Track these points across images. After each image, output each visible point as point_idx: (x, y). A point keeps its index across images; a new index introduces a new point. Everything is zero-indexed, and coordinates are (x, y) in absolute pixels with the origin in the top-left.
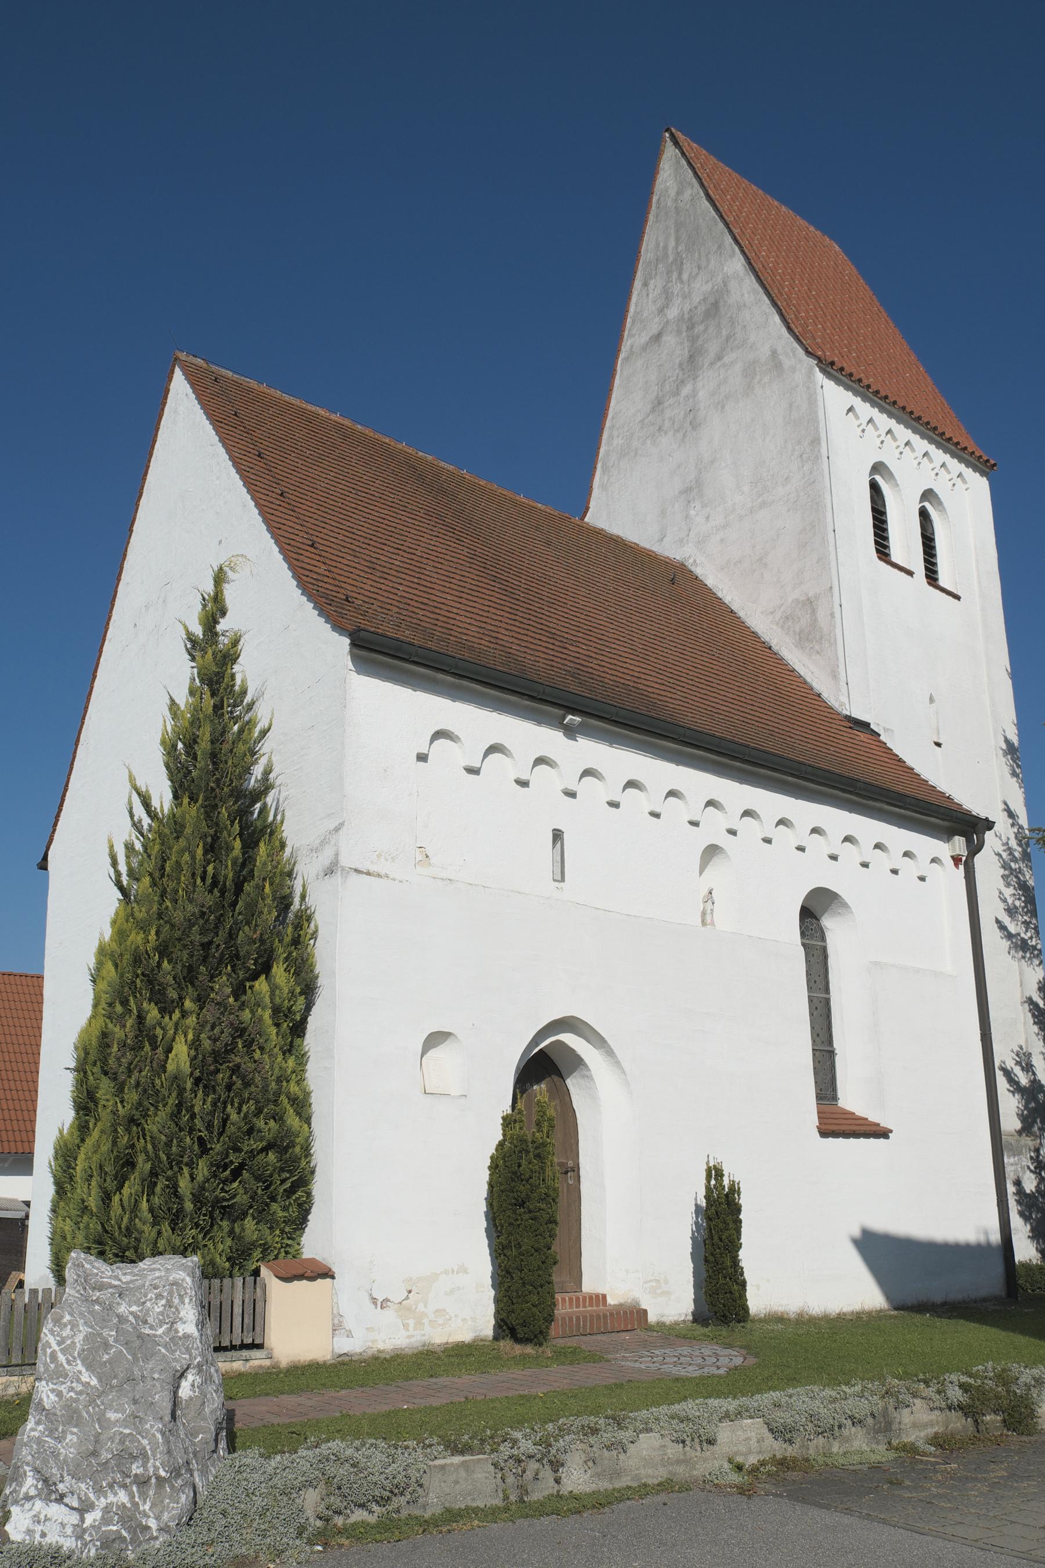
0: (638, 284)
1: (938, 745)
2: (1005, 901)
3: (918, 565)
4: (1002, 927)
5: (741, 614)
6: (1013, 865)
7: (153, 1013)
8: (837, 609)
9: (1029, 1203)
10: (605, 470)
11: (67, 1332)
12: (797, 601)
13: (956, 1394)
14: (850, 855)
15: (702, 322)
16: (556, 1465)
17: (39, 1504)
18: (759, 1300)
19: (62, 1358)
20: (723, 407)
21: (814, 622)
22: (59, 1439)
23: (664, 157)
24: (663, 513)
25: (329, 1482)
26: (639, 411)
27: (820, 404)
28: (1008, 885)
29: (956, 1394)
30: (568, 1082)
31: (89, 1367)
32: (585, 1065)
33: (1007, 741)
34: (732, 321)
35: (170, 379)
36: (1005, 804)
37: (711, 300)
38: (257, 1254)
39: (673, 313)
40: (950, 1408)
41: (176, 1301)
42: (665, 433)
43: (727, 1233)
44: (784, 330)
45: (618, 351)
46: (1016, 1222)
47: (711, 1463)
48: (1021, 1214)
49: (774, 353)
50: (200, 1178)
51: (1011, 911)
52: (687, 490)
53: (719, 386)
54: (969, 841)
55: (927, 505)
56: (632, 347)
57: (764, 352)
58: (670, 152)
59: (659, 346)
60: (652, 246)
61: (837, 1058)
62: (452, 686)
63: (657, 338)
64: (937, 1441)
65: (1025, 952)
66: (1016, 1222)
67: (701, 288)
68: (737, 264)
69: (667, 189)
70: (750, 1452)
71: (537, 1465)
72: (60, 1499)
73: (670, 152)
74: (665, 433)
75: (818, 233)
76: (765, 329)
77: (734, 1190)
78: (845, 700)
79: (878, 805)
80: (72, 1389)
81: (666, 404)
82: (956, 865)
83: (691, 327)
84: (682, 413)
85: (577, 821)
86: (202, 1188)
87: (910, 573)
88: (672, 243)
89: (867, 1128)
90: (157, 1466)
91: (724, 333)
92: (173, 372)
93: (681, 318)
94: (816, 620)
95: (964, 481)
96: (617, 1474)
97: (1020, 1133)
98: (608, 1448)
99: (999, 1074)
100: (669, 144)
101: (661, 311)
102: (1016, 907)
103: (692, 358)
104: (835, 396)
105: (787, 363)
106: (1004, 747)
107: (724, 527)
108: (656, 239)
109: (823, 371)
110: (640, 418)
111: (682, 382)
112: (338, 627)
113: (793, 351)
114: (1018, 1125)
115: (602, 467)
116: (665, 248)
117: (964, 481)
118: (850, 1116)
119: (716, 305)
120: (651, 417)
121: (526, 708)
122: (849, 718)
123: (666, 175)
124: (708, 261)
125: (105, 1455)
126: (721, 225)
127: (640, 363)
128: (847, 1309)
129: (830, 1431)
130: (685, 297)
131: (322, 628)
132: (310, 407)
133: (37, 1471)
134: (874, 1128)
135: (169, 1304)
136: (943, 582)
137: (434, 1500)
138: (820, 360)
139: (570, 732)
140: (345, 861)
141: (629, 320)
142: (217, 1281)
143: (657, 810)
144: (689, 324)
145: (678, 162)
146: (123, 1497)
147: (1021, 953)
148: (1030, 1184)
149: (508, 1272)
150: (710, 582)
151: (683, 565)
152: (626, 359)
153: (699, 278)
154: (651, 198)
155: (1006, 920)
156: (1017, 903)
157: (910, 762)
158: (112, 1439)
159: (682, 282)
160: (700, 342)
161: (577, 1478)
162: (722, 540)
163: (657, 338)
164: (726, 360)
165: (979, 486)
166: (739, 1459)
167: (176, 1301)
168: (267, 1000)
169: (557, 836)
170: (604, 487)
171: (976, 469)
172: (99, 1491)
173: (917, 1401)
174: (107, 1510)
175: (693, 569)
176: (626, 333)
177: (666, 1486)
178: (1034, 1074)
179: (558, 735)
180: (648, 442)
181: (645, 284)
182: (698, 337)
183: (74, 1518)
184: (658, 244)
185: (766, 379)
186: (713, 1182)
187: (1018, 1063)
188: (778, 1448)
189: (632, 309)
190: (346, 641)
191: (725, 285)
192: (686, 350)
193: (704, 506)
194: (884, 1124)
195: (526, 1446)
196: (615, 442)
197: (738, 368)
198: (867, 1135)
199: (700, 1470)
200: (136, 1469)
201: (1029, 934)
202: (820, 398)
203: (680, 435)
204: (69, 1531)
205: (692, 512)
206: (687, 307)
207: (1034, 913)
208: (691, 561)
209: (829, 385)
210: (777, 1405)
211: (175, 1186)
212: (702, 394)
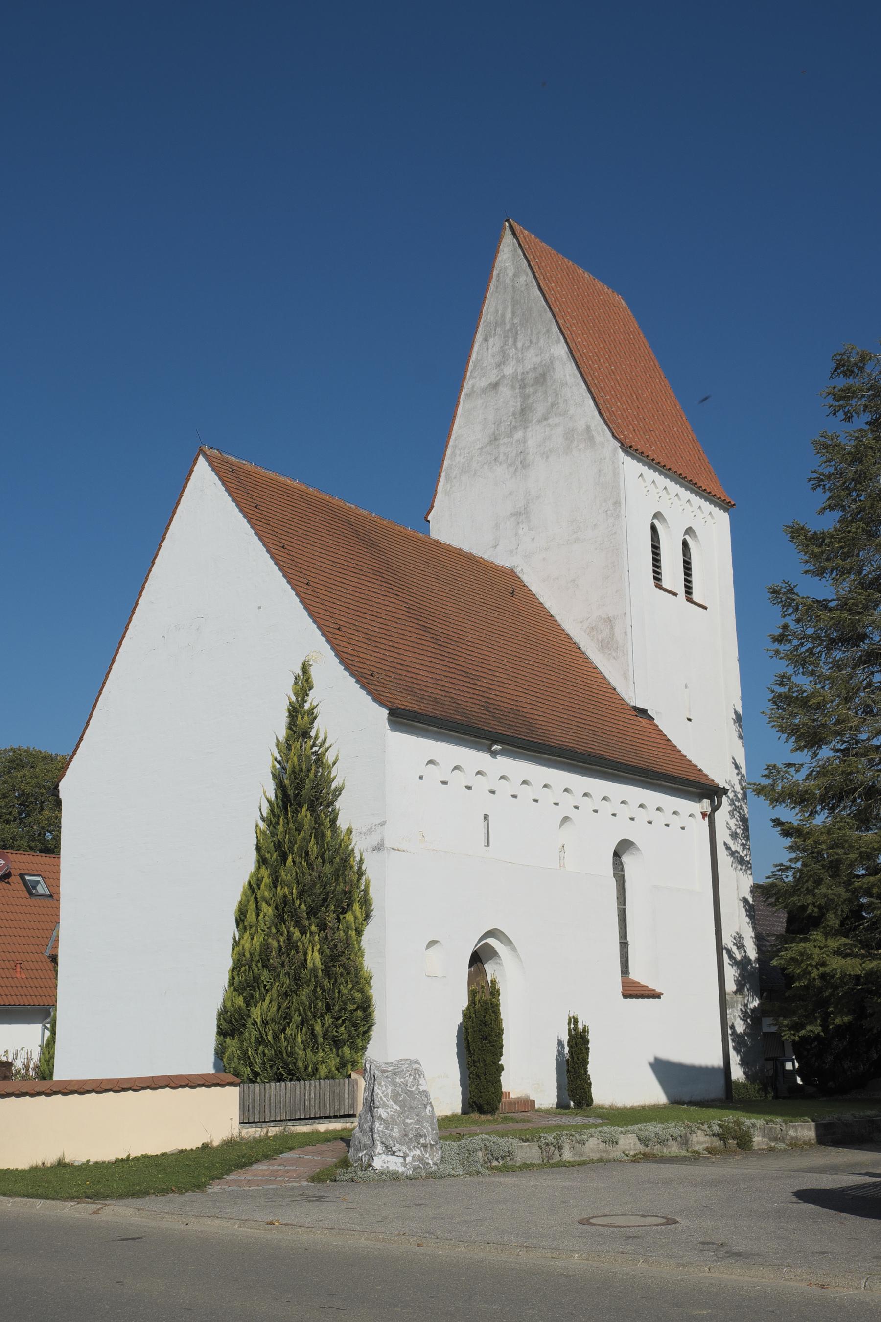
0: (479, 337)
1: (689, 720)
2: (730, 829)
3: (681, 590)
4: (728, 848)
5: (558, 618)
6: (736, 803)
7: (297, 934)
8: (629, 630)
9: (739, 1040)
10: (448, 478)
11: (384, 1089)
13: (716, 1129)
14: (642, 816)
15: (532, 385)
16: (560, 1148)
17: (384, 1155)
19: (384, 1099)
20: (547, 457)
21: (612, 635)
22: (392, 1130)
23: (504, 241)
24: (497, 526)
25: (486, 1149)
26: (479, 440)
27: (622, 476)
28: (733, 816)
29: (716, 1129)
30: (486, 966)
31: (395, 1103)
32: (499, 957)
33: (736, 712)
34: (557, 394)
35: (195, 463)
36: (733, 759)
37: (540, 370)
38: (349, 1067)
39: (508, 370)
40: (714, 1135)
41: (417, 1077)
42: (500, 464)
43: (582, 1055)
44: (596, 413)
45: (462, 387)
46: (733, 1054)
47: (615, 1153)
48: (735, 1048)
49: (588, 428)
50: (326, 1025)
51: (734, 836)
52: (517, 514)
53: (545, 439)
54: (712, 802)
55: (687, 537)
56: (473, 387)
57: (581, 425)
58: (508, 239)
59: (497, 393)
60: (492, 310)
61: (630, 948)
62: (436, 733)
63: (495, 386)
64: (707, 1149)
65: (742, 865)
66: (733, 1054)
67: (531, 359)
68: (560, 350)
69: (506, 268)
70: (631, 1149)
71: (553, 1148)
72: (394, 1153)
73: (508, 239)
74: (500, 464)
75: (610, 291)
76: (583, 410)
77: (585, 1030)
78: (632, 694)
79: (659, 782)
81: (501, 442)
82: (704, 818)
83: (523, 387)
84: (515, 452)
86: (327, 1030)
87: (675, 594)
88: (509, 315)
89: (647, 993)
90: (430, 1140)
91: (550, 400)
92: (197, 459)
93: (514, 377)
94: (613, 634)
95: (712, 517)
96: (581, 1155)
97: (735, 993)
98: (578, 1143)
99: (725, 956)
100: (508, 232)
101: (499, 365)
102: (736, 833)
103: (523, 411)
104: (631, 467)
105: (598, 439)
106: (734, 717)
108: (494, 305)
109: (625, 451)
110: (479, 446)
111: (515, 428)
112: (378, 699)
114: (734, 988)
115: (446, 476)
116: (503, 315)
117: (712, 517)
118: (636, 984)
119: (543, 375)
120: (488, 447)
121: (472, 741)
122: (635, 708)
123: (505, 257)
124: (538, 339)
125: (411, 1136)
126: (550, 315)
127: (480, 401)
128: (636, 1104)
129: (663, 1142)
131: (366, 699)
132: (282, 479)
133: (382, 1143)
134: (653, 993)
135: (415, 1078)
136: (696, 597)
137: (519, 1160)
138: (622, 444)
139: (494, 754)
140: (387, 844)
141: (471, 363)
142: (283, 1083)
143: (537, 798)
144: (521, 383)
145: (515, 250)
146: (418, 1152)
147: (739, 867)
148: (740, 1028)
149: (478, 1076)
150: (534, 589)
151: (512, 571)
152: (468, 395)
153: (531, 350)
154: (492, 271)
155: (730, 842)
156: (738, 831)
157: (675, 741)
158: (411, 1129)
159: (516, 348)
160: (530, 401)
161: (568, 1155)
162: (544, 559)
164: (550, 421)
165: (723, 518)
166: (627, 1152)
167: (417, 1077)
168: (353, 925)
169: (486, 817)
170: (447, 493)
171: (721, 507)
172: (410, 1149)
173: (700, 1131)
174: (413, 1157)
175: (520, 575)
176: (468, 374)
177: (600, 1160)
178: (745, 952)
179: (486, 756)
180: (486, 467)
181: (486, 340)
182: (529, 396)
183: (401, 1160)
184: (497, 311)
187: (735, 944)
188: (641, 1148)
189: (474, 356)
190: (386, 712)
191: (552, 363)
192: (519, 404)
194: (658, 990)
195: (550, 1139)
196: (458, 459)
197: (560, 430)
198: (649, 997)
199: (612, 1155)
200: (422, 1141)
201: (745, 853)
202: (621, 472)
203: (512, 469)
204: (399, 1165)
205: (521, 532)
207: (747, 838)
209: (628, 460)
210: (641, 1130)
211: (313, 1030)
212: (531, 443)
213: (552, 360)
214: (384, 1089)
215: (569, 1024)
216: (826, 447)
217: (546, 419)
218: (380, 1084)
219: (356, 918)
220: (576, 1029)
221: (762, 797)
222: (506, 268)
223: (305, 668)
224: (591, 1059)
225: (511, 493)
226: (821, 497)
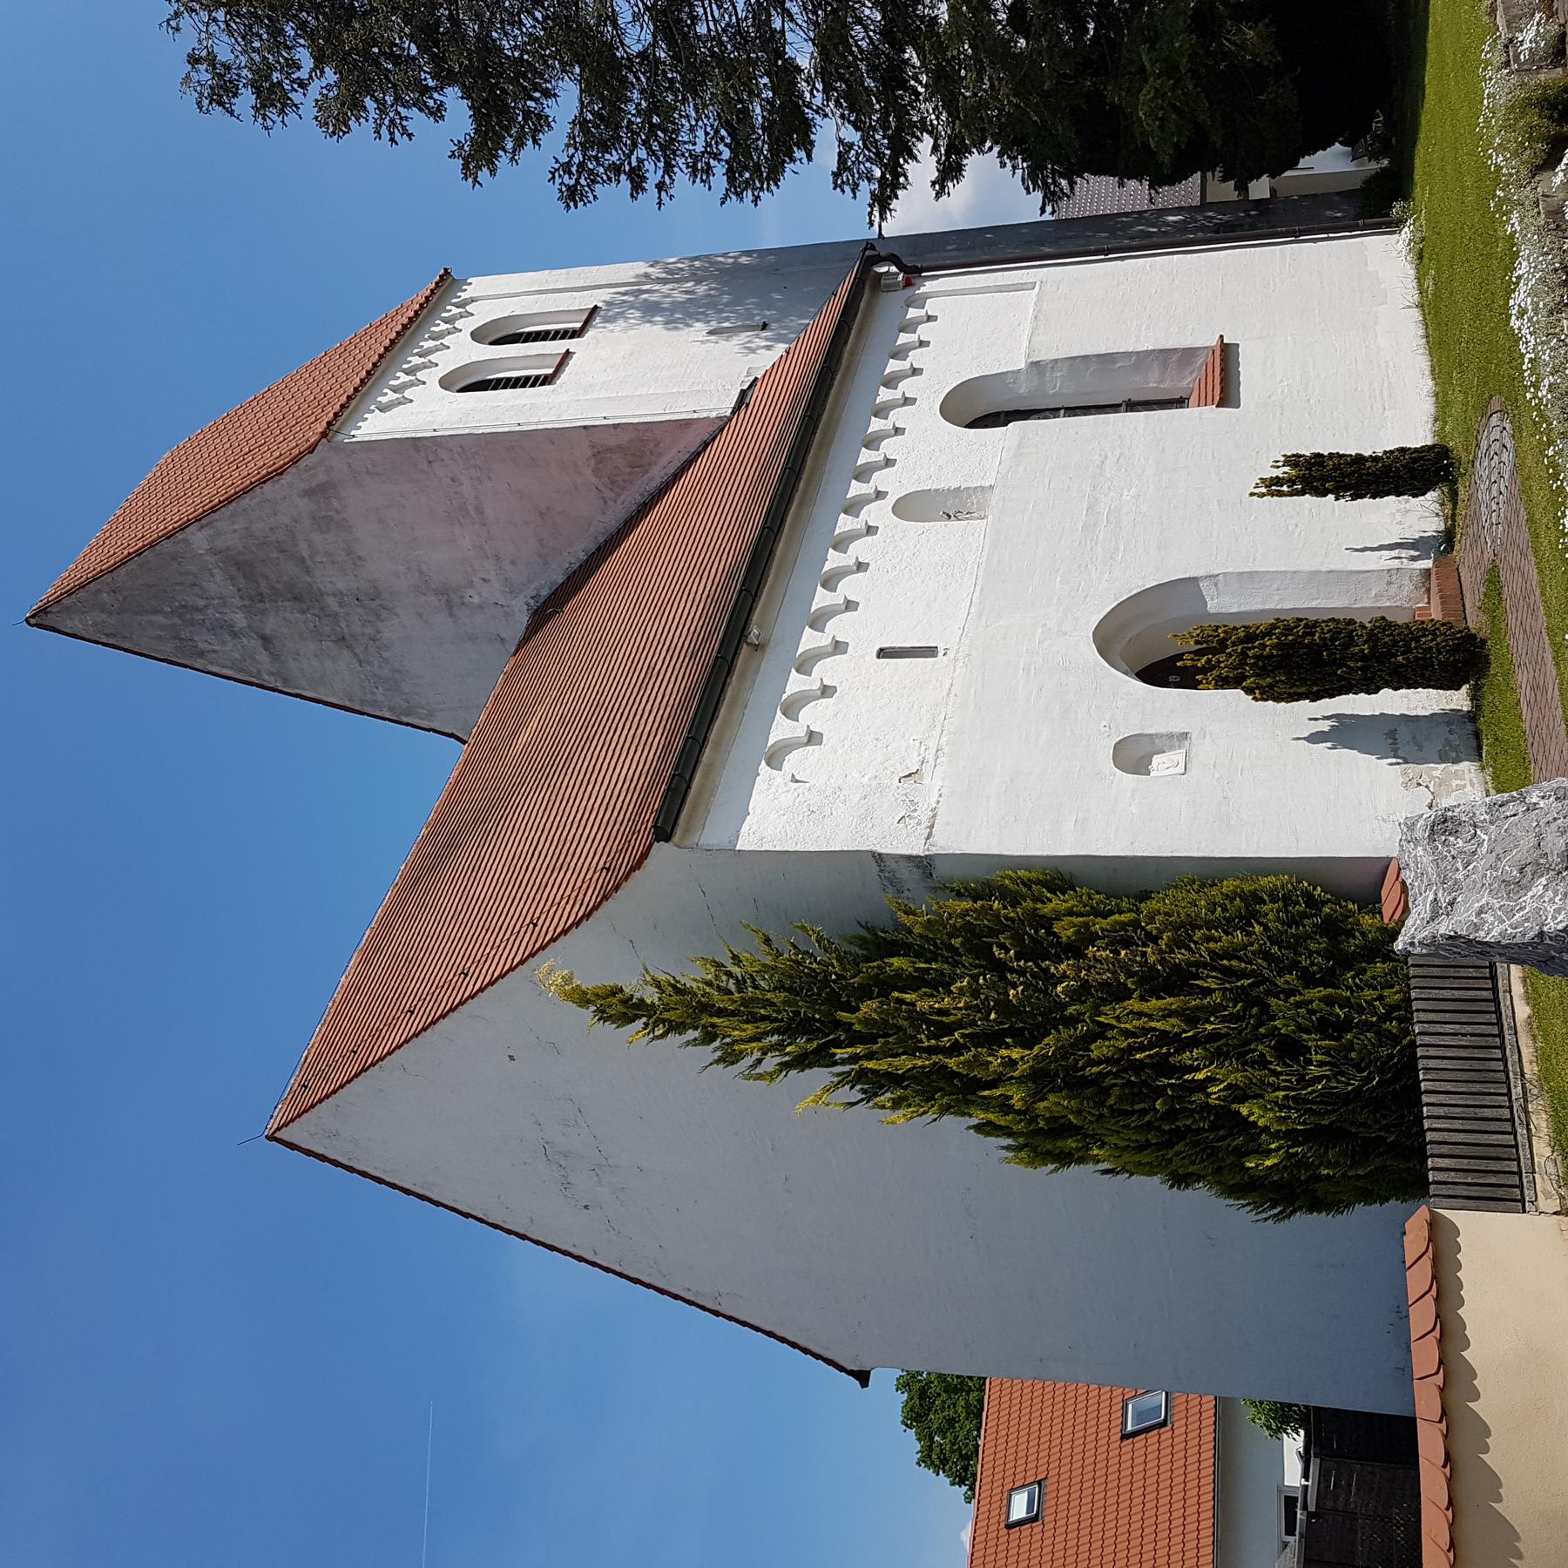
12: (596, 471)
18: (1418, 435)
20: (360, 558)
24: (472, 638)
39: (240, 620)
49: (308, 493)
52: (450, 607)
56: (272, 674)
57: (304, 505)
63: (266, 640)
67: (217, 583)
77: (1293, 461)
79: (846, 356)
80: (1552, 901)
84: (360, 610)
85: (894, 483)
88: (159, 618)
94: (620, 447)
103: (296, 598)
107: (497, 557)
113: (308, 468)
116: (162, 628)
119: (240, 565)
130: (224, 604)
144: (256, 601)
162: (513, 563)
163: (266, 640)
164: (305, 554)
180: (386, 654)
182: (272, 588)
185: (336, 504)
186: (1285, 488)
193: (471, 584)
196: (380, 698)
197: (317, 538)
203: (384, 614)
205: (476, 600)
206: (238, 602)
208: (532, 602)
213: (213, 552)
214: (1488, 917)
215: (1280, 494)
216: (337, 118)
217: (303, 561)
218: (1477, 927)
219: (1070, 913)
220: (1291, 481)
221: (894, 204)
222: (95, 624)
223: (583, 999)
224: (1351, 450)
225: (420, 616)
226: (416, 119)
